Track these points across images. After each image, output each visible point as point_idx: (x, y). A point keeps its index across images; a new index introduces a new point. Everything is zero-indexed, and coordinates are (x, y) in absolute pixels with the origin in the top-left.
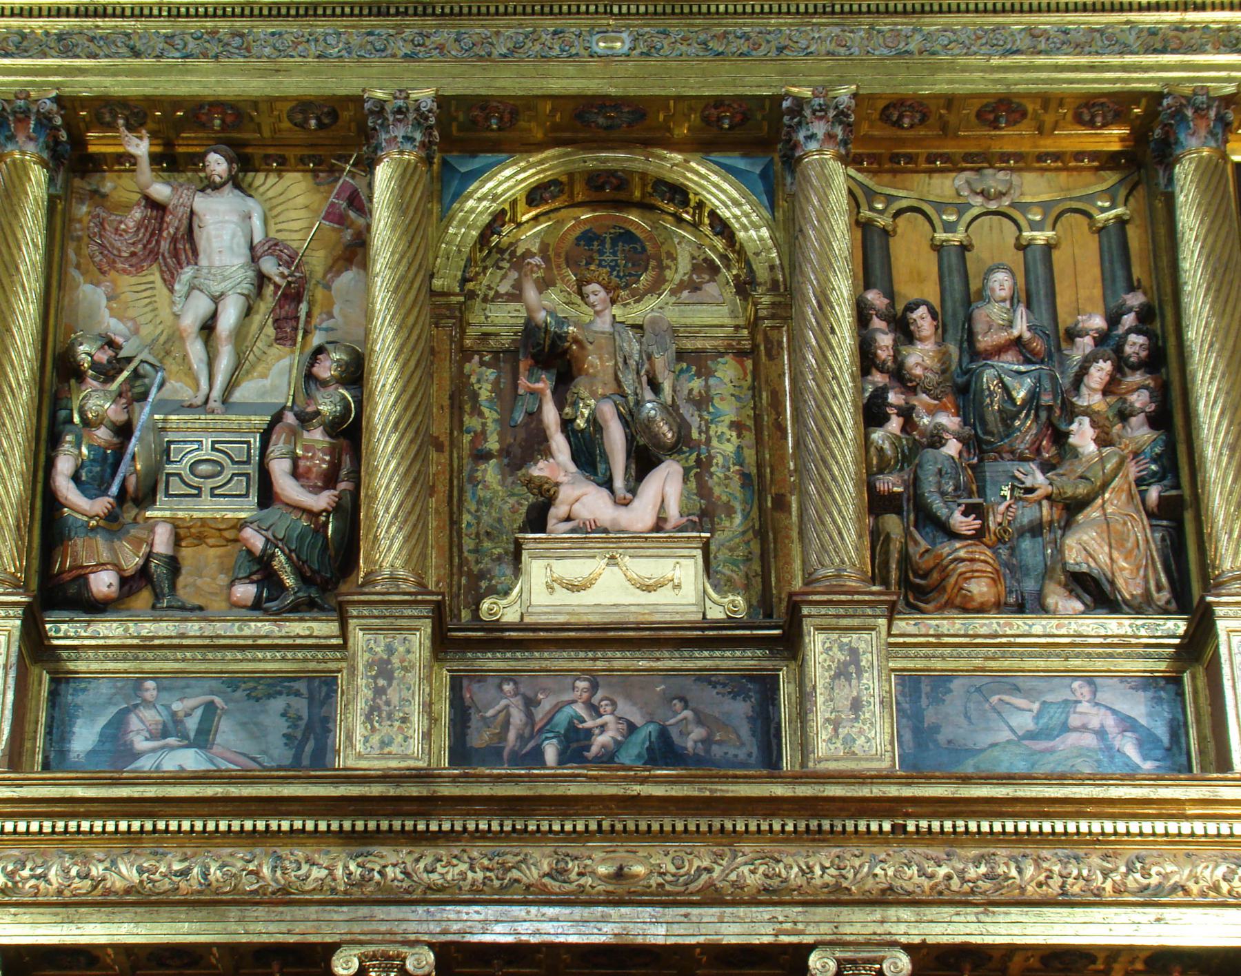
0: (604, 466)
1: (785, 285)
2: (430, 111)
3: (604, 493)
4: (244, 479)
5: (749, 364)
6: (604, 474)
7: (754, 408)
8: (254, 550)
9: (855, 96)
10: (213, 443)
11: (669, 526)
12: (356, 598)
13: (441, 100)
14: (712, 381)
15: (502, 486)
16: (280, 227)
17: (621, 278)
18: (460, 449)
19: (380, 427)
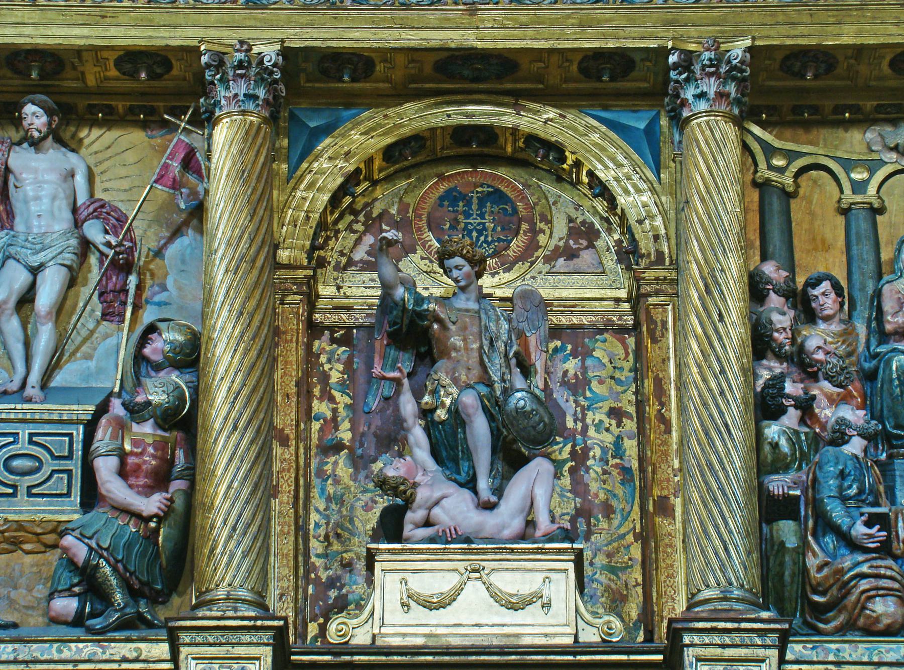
0: (467, 464)
1: (671, 257)
2: (274, 66)
3: (466, 494)
4: (65, 476)
5: (631, 341)
6: (468, 473)
7: (636, 393)
8: (76, 560)
9: (749, 49)
10: (31, 435)
11: (539, 533)
12: (188, 623)
13: (286, 53)
14: (589, 362)
15: (355, 480)
16: (107, 185)
17: (489, 244)
18: (308, 438)
19: (217, 426)
